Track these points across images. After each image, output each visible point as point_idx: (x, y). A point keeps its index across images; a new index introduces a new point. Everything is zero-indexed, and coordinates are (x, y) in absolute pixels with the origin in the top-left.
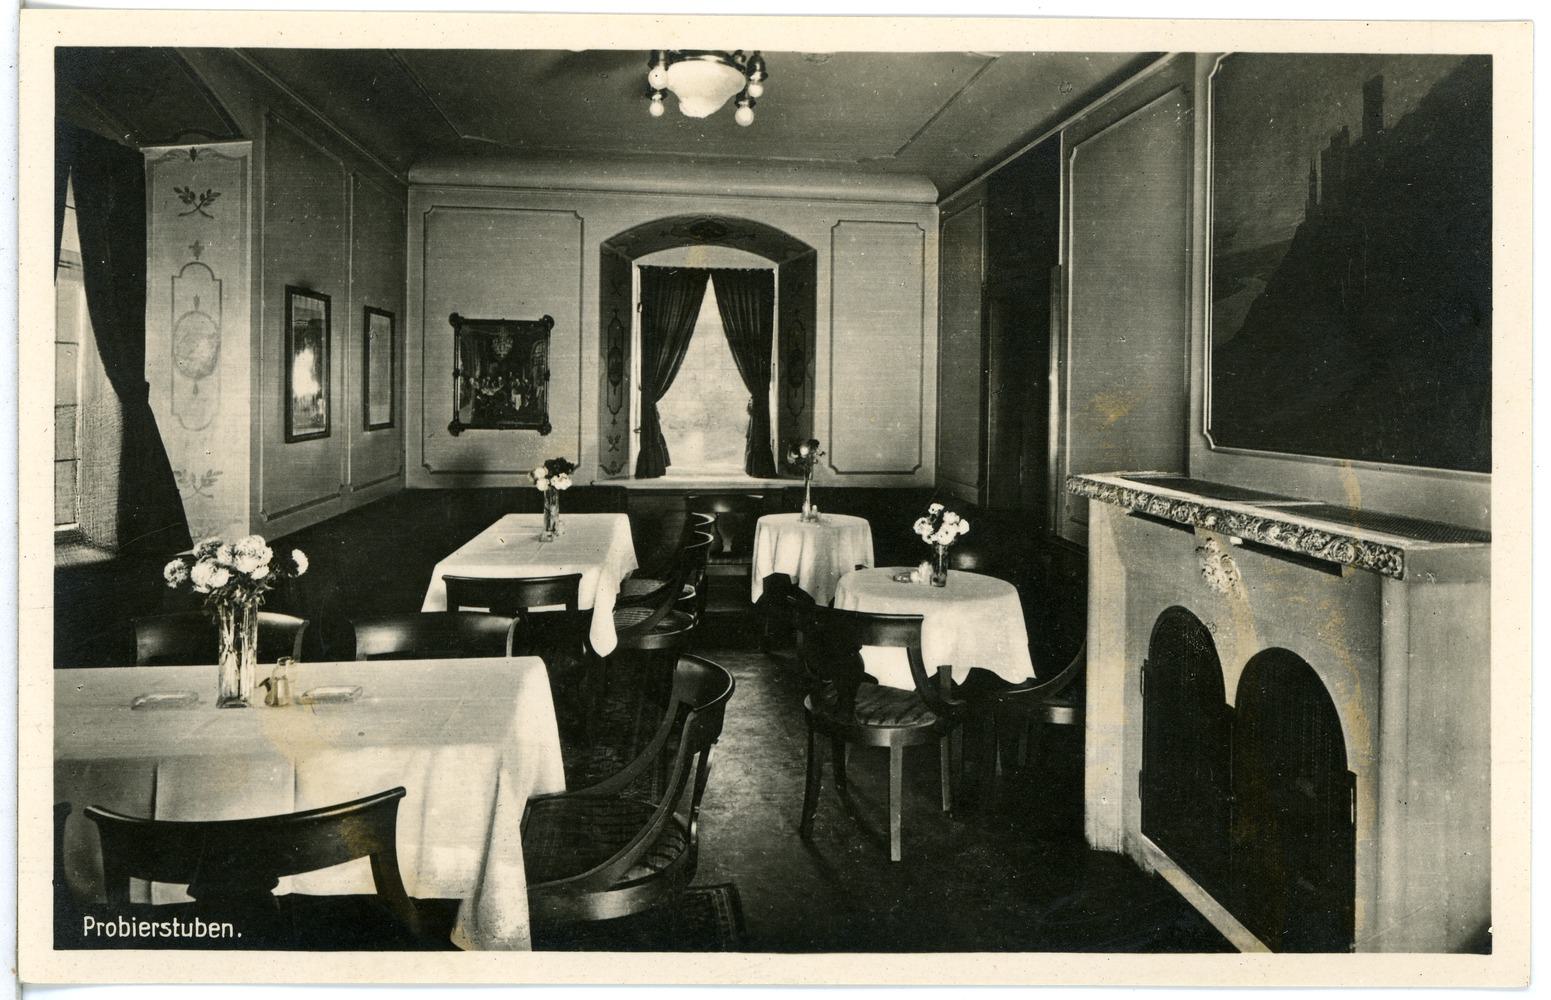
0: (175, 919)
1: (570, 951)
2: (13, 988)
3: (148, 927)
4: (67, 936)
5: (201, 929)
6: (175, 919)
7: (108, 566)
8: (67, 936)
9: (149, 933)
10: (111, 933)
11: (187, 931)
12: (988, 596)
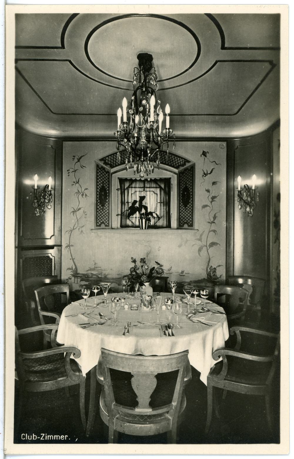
1: (246, 443)
2: (2, 455)
3: (64, 437)
4: (18, 440)
8: (18, 440)
9: (64, 439)
10: (23, 438)
11: (30, 438)
12: (176, 15)
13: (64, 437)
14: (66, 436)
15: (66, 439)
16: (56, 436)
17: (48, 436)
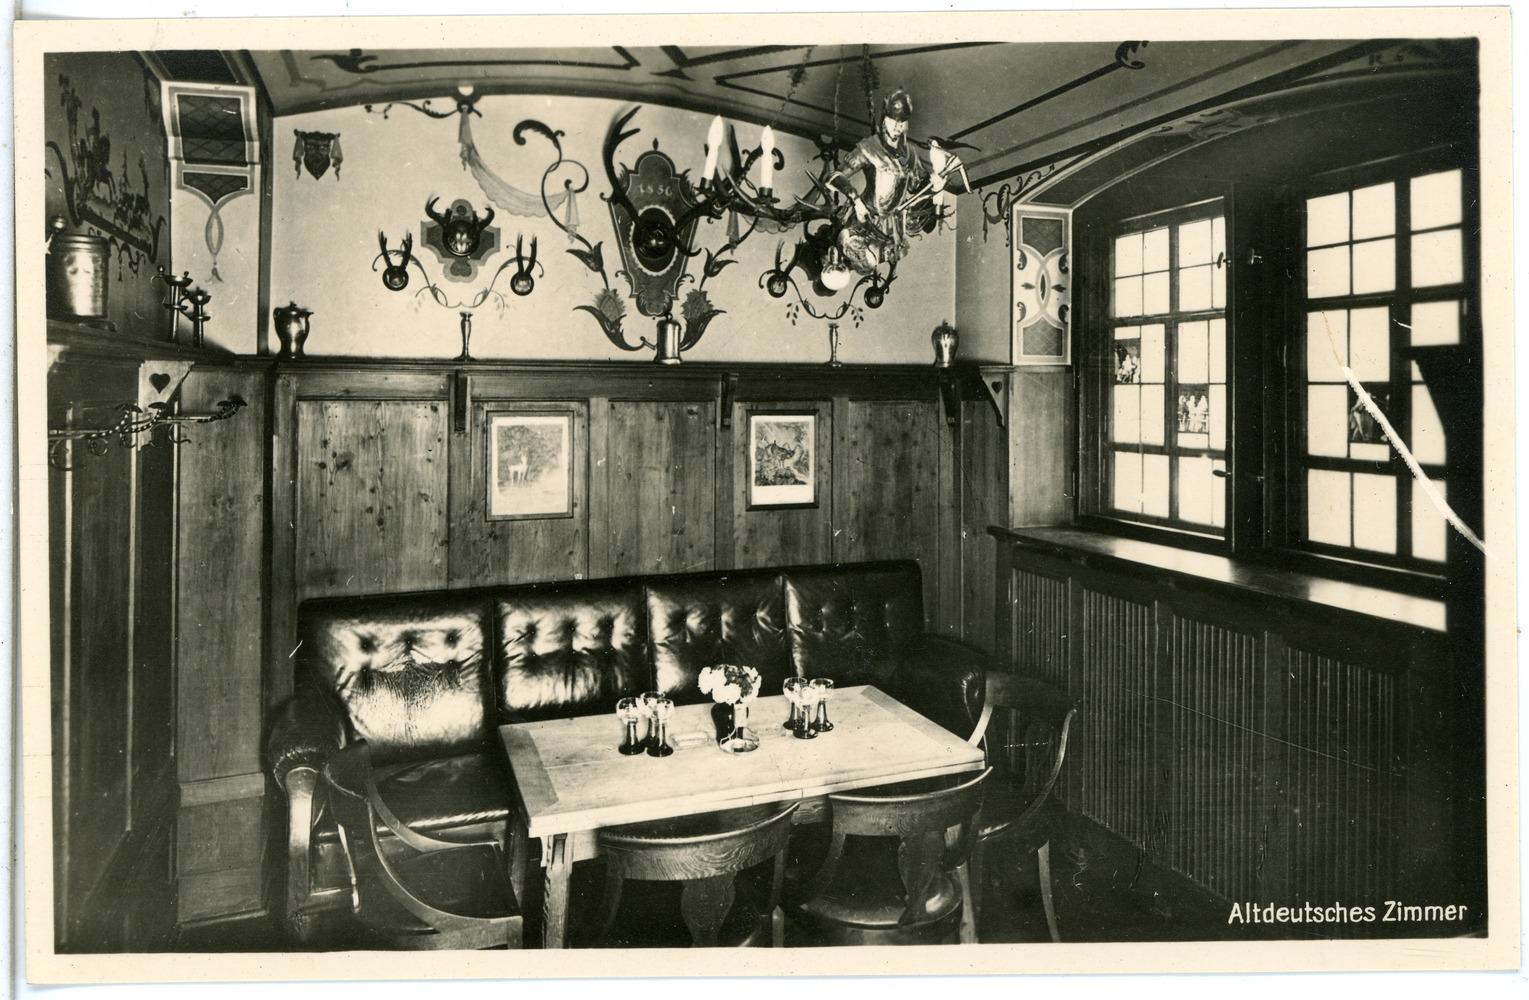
0: (1307, 904)
3: (1455, 911)
5: (1312, 914)
6: (1307, 904)
7: (53, 461)
9: (1455, 917)
11: (1297, 916)
13: (1455, 911)
14: (1461, 908)
15: (1461, 917)
16: (1410, 908)
17: (1406, 909)
